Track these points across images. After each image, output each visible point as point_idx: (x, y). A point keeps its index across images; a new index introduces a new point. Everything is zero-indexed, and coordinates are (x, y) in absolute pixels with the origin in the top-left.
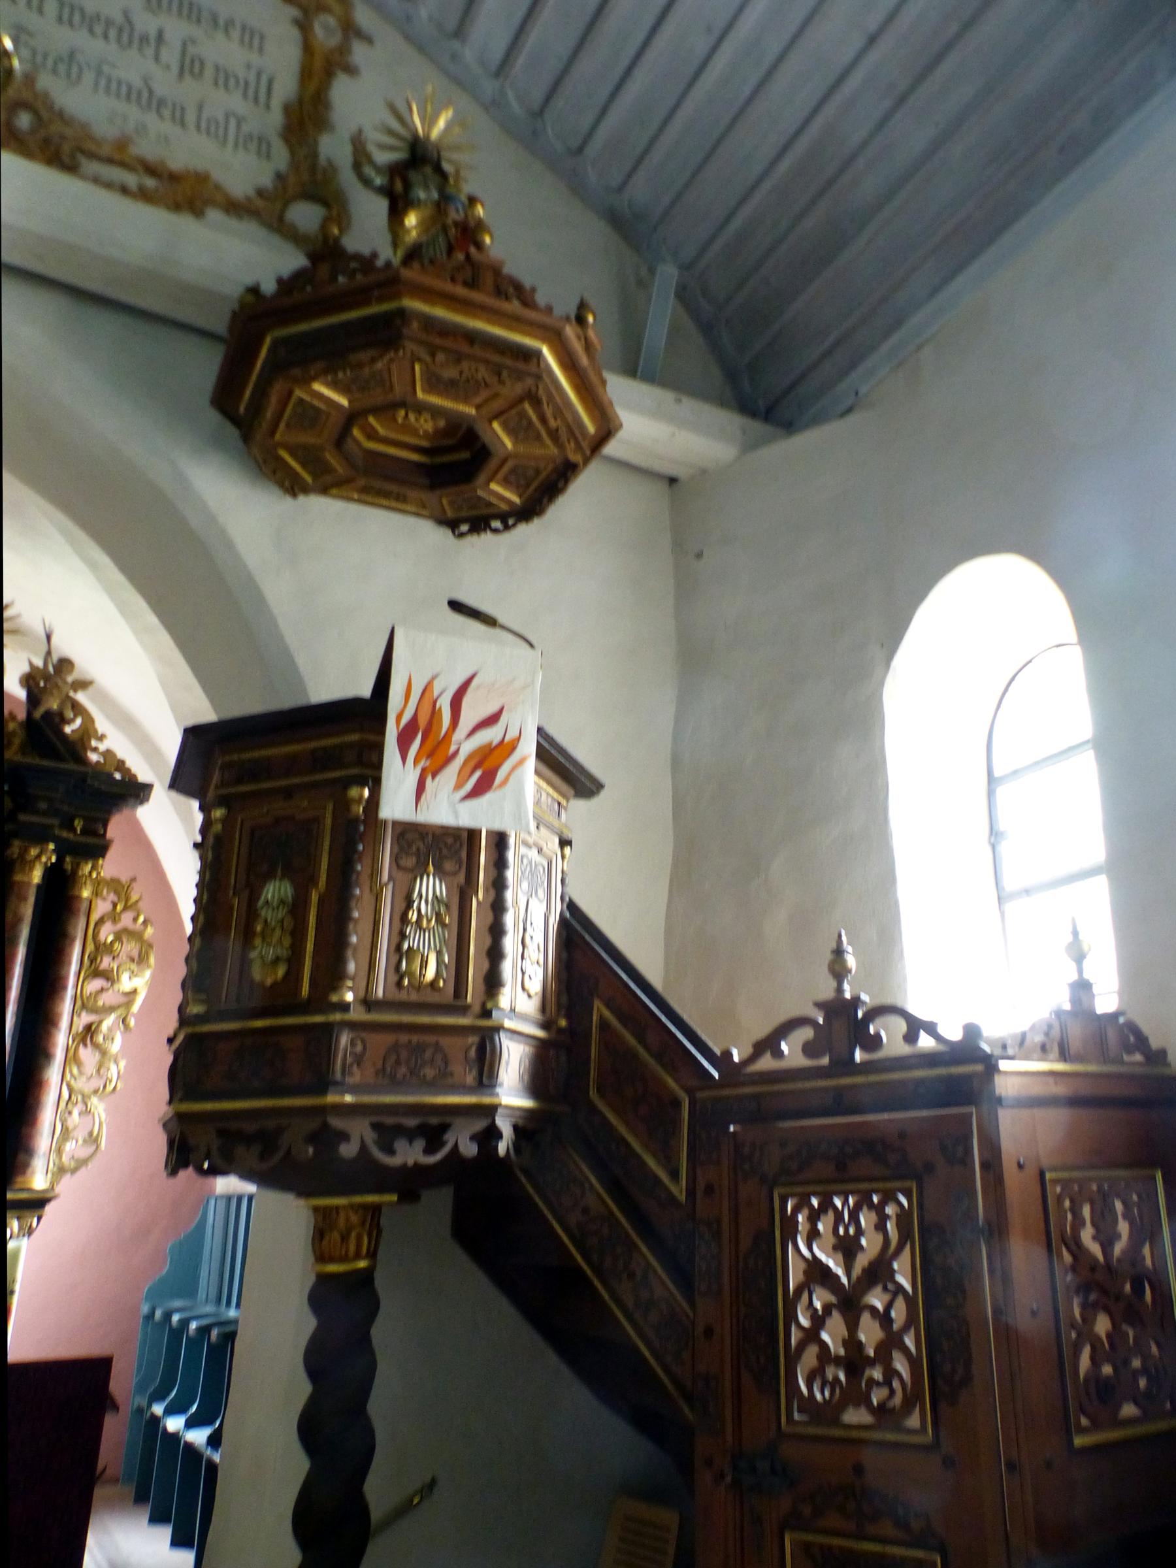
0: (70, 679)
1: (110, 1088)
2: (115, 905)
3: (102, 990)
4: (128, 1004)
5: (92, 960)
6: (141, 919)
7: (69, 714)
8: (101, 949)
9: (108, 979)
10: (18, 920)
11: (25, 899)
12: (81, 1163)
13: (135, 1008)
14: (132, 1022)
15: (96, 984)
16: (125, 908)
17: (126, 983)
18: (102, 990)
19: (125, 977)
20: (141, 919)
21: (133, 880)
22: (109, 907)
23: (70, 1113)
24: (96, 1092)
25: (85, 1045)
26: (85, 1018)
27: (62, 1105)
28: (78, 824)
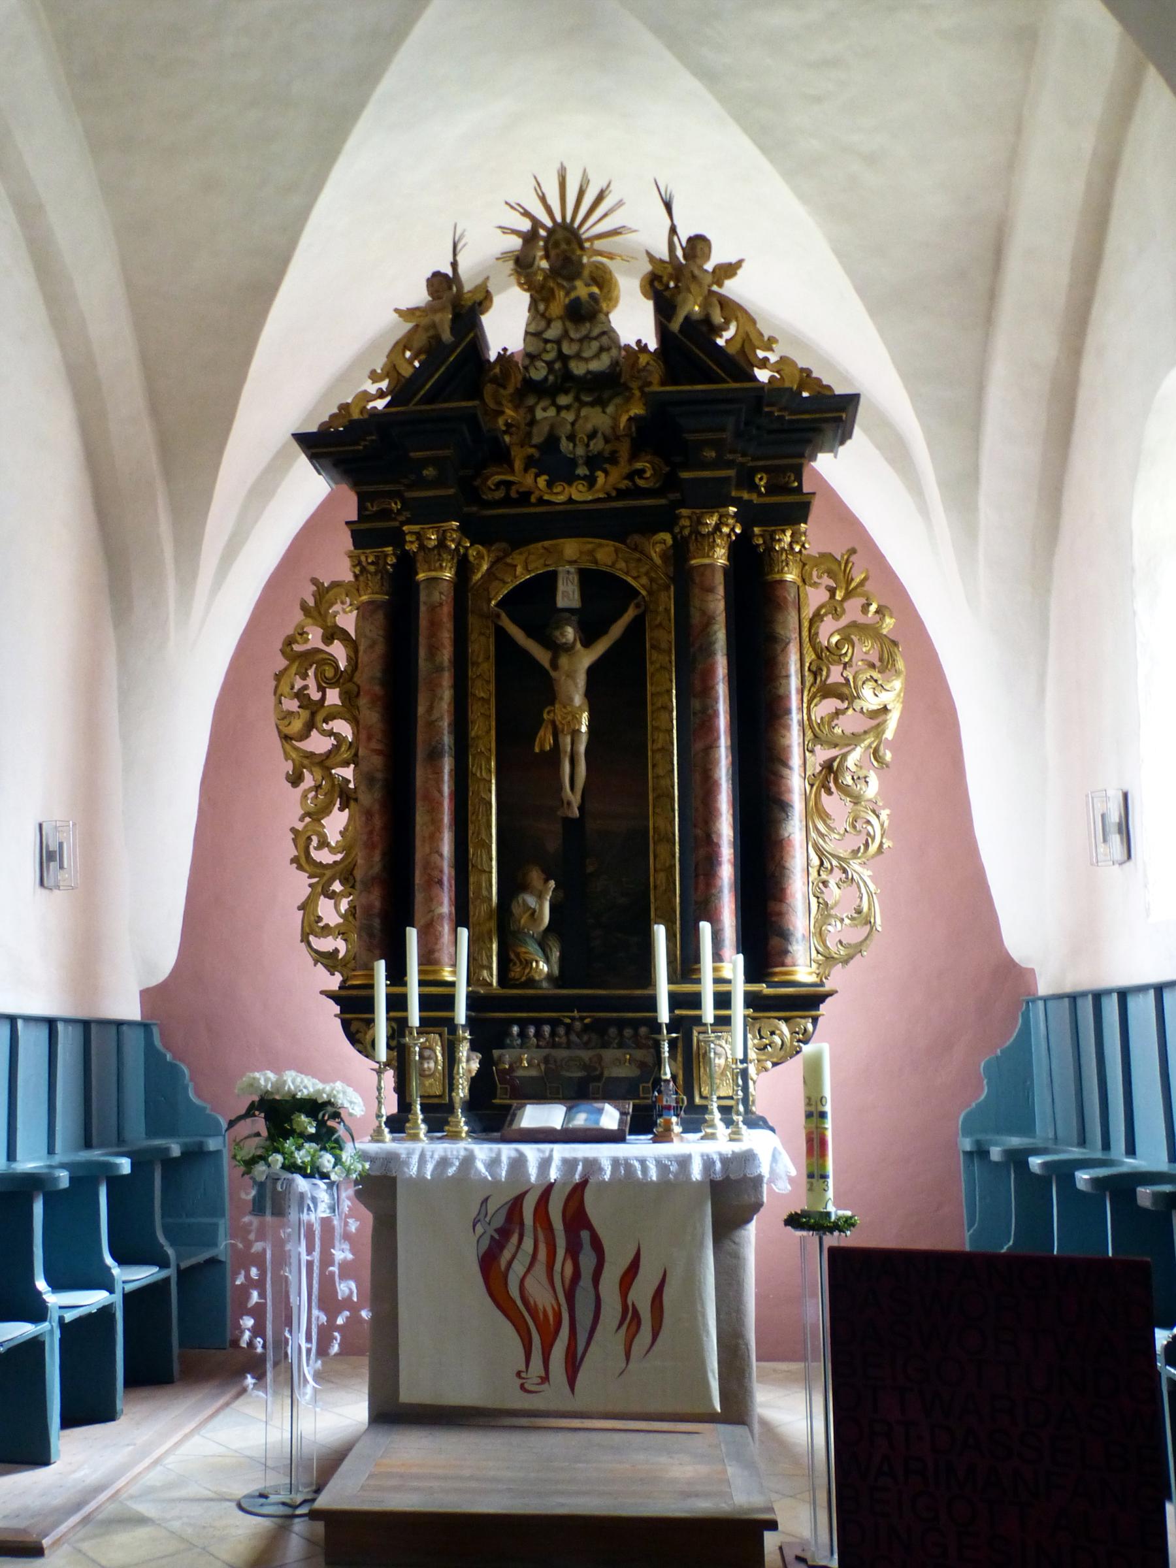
0: (709, 266)
1: (873, 848)
2: (832, 591)
3: (838, 713)
4: (878, 729)
5: (816, 674)
6: (873, 608)
7: (718, 319)
8: (825, 656)
9: (842, 697)
10: (709, 621)
11: (711, 590)
12: (856, 950)
13: (889, 734)
14: (888, 756)
15: (826, 707)
16: (848, 595)
17: (870, 699)
18: (838, 713)
19: (867, 691)
20: (873, 608)
21: (853, 551)
22: (824, 596)
23: (825, 883)
24: (855, 853)
25: (829, 792)
26: (823, 754)
27: (813, 872)
28: (762, 481)
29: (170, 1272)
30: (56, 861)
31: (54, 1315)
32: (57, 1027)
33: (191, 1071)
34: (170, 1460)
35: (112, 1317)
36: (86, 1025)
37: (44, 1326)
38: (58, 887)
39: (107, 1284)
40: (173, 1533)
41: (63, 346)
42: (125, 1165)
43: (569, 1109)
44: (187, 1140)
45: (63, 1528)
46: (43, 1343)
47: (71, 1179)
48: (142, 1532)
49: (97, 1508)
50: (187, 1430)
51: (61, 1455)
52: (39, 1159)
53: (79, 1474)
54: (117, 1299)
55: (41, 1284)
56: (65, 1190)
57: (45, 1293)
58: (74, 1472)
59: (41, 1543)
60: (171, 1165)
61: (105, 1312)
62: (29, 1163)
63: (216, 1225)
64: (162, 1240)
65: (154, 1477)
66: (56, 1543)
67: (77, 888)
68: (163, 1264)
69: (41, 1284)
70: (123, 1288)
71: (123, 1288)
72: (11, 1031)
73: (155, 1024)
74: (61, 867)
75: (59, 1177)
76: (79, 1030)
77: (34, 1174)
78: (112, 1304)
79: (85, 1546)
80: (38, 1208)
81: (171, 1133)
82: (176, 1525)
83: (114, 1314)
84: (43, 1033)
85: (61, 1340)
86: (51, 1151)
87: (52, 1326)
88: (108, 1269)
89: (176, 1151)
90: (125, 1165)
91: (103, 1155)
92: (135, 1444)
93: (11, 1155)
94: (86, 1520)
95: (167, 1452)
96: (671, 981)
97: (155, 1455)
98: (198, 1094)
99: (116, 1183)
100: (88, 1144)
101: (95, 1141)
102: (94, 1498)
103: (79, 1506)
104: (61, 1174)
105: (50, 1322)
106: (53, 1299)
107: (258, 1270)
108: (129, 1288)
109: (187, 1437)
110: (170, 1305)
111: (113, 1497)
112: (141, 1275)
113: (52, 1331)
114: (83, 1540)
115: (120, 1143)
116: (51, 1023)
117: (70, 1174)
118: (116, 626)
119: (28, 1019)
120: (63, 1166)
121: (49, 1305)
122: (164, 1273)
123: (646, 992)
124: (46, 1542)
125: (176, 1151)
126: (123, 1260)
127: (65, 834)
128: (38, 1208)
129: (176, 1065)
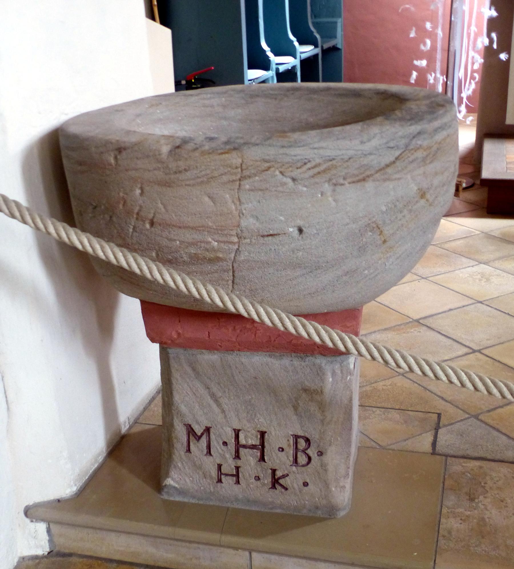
29: (318, 51)
31: (274, 67)
39: (293, 54)
43: (175, 467)
63: (336, 23)
106: (274, 59)
107: (432, 23)
108: (304, 56)
110: (319, 73)
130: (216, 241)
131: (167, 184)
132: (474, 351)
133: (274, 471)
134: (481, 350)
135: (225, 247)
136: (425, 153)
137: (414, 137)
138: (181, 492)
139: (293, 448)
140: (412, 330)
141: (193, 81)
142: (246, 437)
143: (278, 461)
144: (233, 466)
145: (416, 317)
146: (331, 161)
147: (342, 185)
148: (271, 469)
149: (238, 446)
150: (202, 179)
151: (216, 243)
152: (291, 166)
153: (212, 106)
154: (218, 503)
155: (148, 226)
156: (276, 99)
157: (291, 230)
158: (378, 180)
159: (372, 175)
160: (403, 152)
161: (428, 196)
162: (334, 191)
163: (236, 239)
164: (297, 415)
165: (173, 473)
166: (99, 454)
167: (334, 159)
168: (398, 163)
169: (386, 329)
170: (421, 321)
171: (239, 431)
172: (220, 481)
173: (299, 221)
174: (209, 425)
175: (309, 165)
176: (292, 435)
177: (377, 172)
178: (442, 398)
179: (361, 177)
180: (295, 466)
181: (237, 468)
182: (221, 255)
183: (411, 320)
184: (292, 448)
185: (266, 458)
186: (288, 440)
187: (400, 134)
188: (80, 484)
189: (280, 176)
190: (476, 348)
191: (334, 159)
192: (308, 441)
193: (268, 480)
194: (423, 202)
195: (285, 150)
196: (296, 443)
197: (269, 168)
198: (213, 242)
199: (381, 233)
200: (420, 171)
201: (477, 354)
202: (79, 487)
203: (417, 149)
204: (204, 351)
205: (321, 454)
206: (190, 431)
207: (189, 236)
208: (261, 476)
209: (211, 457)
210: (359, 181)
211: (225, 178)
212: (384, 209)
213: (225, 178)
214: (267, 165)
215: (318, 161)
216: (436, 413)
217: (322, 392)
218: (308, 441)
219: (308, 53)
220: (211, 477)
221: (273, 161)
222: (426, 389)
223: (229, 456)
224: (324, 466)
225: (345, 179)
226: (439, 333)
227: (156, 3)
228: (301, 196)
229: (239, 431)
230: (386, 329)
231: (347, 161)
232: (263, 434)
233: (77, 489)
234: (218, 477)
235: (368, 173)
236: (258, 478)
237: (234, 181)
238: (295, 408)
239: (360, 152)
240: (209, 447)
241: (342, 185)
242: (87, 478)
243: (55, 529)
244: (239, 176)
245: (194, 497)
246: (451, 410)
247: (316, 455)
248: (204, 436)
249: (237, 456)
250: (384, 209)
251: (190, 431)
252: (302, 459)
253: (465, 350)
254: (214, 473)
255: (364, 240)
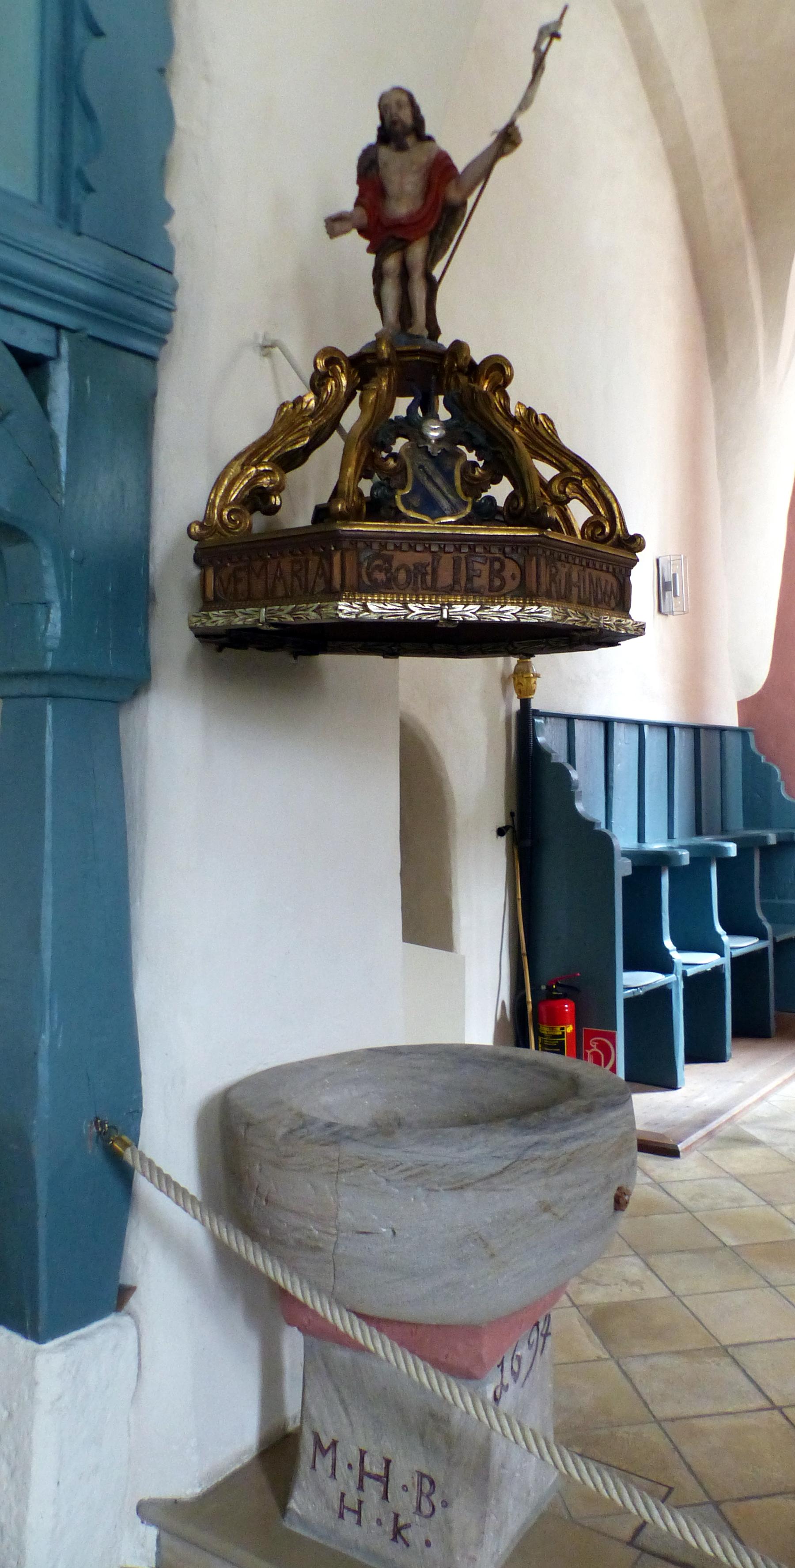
30: (671, 590)
31: (679, 969)
32: (674, 731)
33: (782, 771)
34: (774, 1099)
35: (723, 976)
36: (696, 731)
37: (671, 978)
38: (672, 613)
39: (717, 948)
40: (782, 1155)
41: (663, 133)
42: (732, 849)
44: (781, 831)
45: (693, 1138)
46: (670, 991)
47: (691, 859)
48: (756, 1151)
49: (718, 1127)
50: (779, 1081)
51: (686, 1083)
52: (661, 842)
53: (700, 1100)
54: (726, 961)
55: (668, 943)
56: (685, 867)
57: (672, 951)
58: (697, 1097)
59: (676, 1146)
60: (767, 850)
61: (717, 971)
62: (656, 844)
64: (760, 915)
65: (762, 1110)
66: (688, 1149)
67: (688, 613)
68: (762, 936)
69: (668, 943)
70: (731, 953)
71: (731, 953)
72: (639, 733)
73: (751, 731)
74: (675, 595)
75: (681, 855)
76: (690, 734)
77: (662, 852)
78: (722, 965)
79: (711, 1155)
80: (665, 880)
81: (768, 825)
82: (784, 1149)
83: (724, 975)
84: (663, 736)
85: (685, 990)
86: (670, 836)
87: (677, 978)
88: (719, 936)
89: (772, 840)
90: (732, 849)
91: (711, 840)
92: (743, 1082)
93: (641, 838)
94: (710, 1135)
95: (771, 1092)
96: (564, 1041)
97: (763, 1091)
98: (788, 791)
99: (724, 863)
100: (699, 832)
101: (704, 831)
102: (715, 1119)
103: (704, 1123)
104: (684, 853)
105: (676, 975)
106: (679, 957)
108: (736, 953)
109: (786, 1082)
111: (730, 1120)
112: (745, 944)
113: (677, 982)
114: (709, 1149)
115: (724, 831)
116: (669, 728)
117: (633, 862)
118: (714, 380)
119: (652, 725)
120: (682, 847)
121: (675, 960)
122: (763, 945)
123: (614, 1031)
124: (681, 1147)
125: (772, 840)
126: (732, 931)
127: (677, 567)
128: (665, 880)
129: (770, 767)
130: (318, 1230)
131: (277, 1165)
132: (773, 1407)
133: (397, 1516)
134: (785, 1407)
135: (325, 1237)
136: (546, 1165)
137: (529, 1147)
138: (304, 1522)
139: (418, 1489)
140: (710, 1361)
141: (554, 987)
142: (371, 1464)
143: (401, 1503)
144: (356, 1499)
145: (726, 1341)
146: (424, 1165)
147: (437, 1191)
148: (394, 1513)
149: (363, 1473)
150: (305, 1167)
151: (317, 1232)
152: (383, 1166)
153: (419, 1068)
154: (338, 1548)
155: (264, 1203)
156: (484, 1067)
157: (384, 1230)
158: (480, 1190)
159: (472, 1184)
160: (514, 1162)
161: (555, 1210)
162: (428, 1196)
163: (334, 1231)
164: (423, 1445)
165: (296, 1493)
166: (244, 1453)
167: (427, 1164)
168: (506, 1174)
169: (678, 1353)
170: (730, 1350)
171: (365, 1452)
172: (341, 1516)
173: (391, 1222)
174: (336, 1439)
175: (401, 1168)
176: (418, 1472)
177: (480, 1180)
178: (689, 1468)
179: (458, 1185)
180: (419, 1515)
181: (360, 1503)
182: (321, 1245)
183: (718, 1345)
184: (416, 1488)
185: (389, 1496)
186: (413, 1477)
187: (511, 1143)
188: (207, 1486)
189: (374, 1175)
190: (778, 1401)
191: (427, 1164)
192: (432, 1483)
193: (389, 1528)
194: (546, 1216)
195: (378, 1151)
196: (420, 1484)
197: (362, 1166)
198: (315, 1230)
199: (486, 1246)
200: (543, 1181)
201: (776, 1412)
202: (206, 1489)
203: (533, 1160)
204: (336, 1345)
205: (445, 1504)
206: (318, 1442)
207: (295, 1221)
208: (384, 1519)
209: (335, 1481)
210: (454, 1189)
211: (324, 1169)
212: (489, 1220)
213: (324, 1169)
214: (362, 1162)
215: (410, 1164)
216: (668, 1487)
217: (449, 1421)
218: (432, 1483)
219: (744, 949)
220: (334, 1510)
221: (366, 1159)
222: (676, 1448)
223: (353, 1484)
224: (448, 1522)
225: (440, 1185)
226: (744, 1371)
227: (520, 897)
228: (393, 1197)
229: (365, 1452)
230: (678, 1353)
231: (442, 1168)
232: (388, 1462)
233: (201, 1491)
234: (340, 1512)
235: (467, 1181)
236: (379, 1522)
237: (332, 1173)
238: (422, 1436)
239: (457, 1160)
240: (334, 1466)
241: (437, 1191)
242: (220, 1479)
243: (165, 1538)
244: (335, 1170)
245: (314, 1532)
246: (690, 1484)
247: (440, 1505)
248: (330, 1452)
249: (361, 1487)
250: (489, 1220)
251: (318, 1442)
252: (426, 1508)
253: (762, 1403)
254: (336, 1504)
255: (465, 1251)
